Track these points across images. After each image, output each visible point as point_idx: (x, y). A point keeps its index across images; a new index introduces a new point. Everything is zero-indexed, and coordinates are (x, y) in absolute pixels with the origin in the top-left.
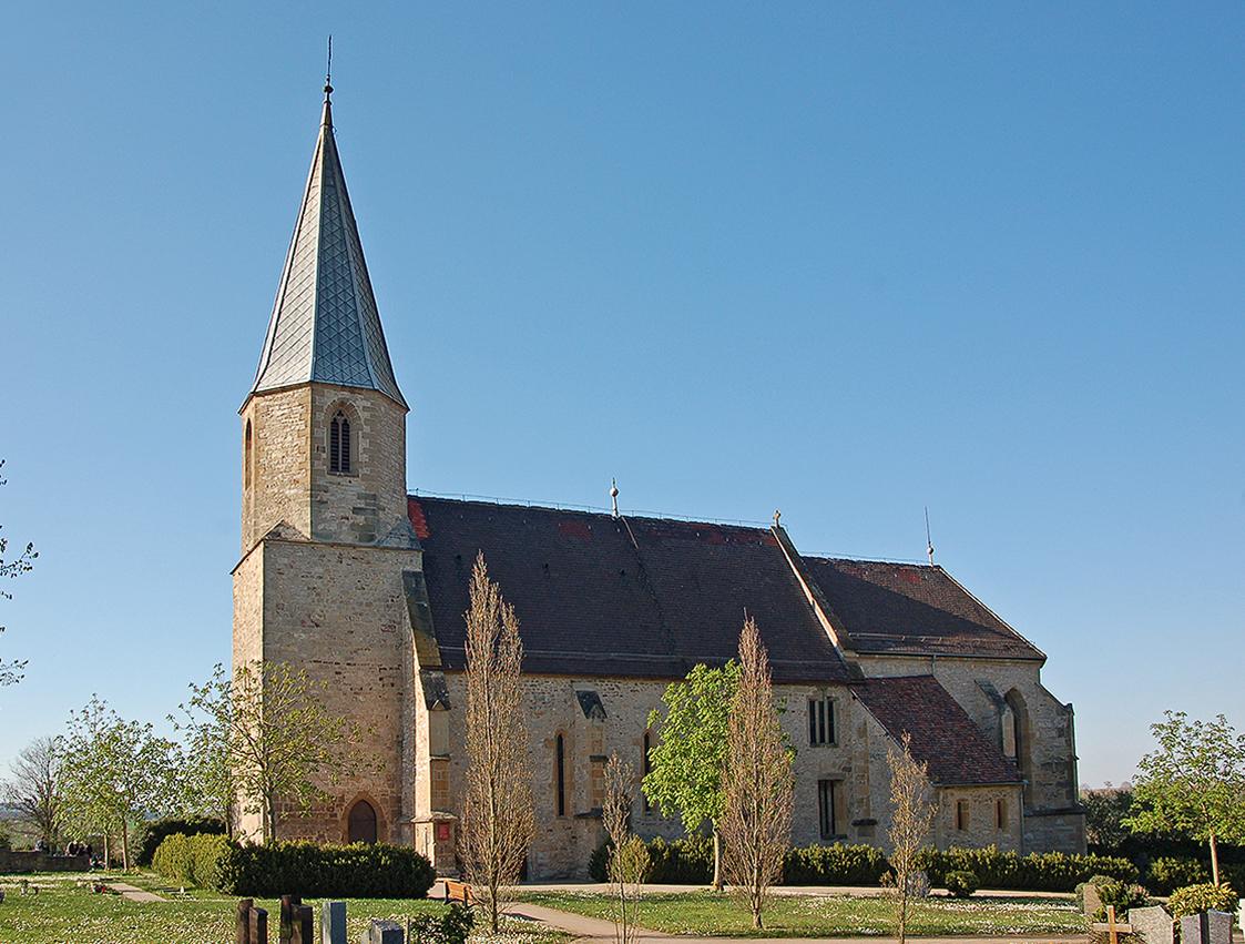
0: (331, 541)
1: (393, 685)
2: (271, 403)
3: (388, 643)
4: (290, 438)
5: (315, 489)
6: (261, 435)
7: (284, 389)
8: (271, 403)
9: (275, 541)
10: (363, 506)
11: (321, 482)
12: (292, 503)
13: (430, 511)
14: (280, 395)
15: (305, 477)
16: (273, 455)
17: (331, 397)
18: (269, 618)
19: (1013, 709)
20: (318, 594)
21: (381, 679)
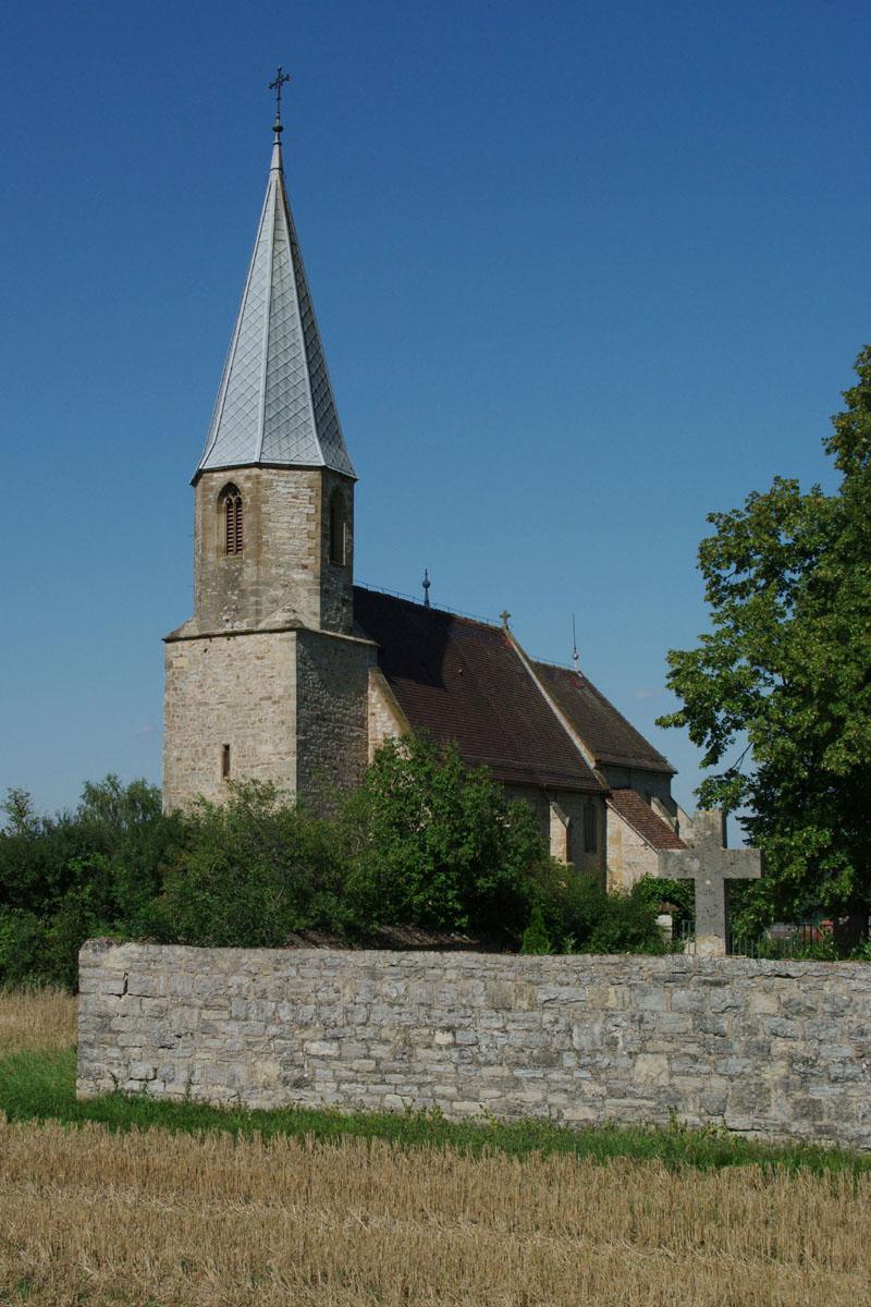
2: (276, 478)
14: (286, 472)
15: (314, 561)
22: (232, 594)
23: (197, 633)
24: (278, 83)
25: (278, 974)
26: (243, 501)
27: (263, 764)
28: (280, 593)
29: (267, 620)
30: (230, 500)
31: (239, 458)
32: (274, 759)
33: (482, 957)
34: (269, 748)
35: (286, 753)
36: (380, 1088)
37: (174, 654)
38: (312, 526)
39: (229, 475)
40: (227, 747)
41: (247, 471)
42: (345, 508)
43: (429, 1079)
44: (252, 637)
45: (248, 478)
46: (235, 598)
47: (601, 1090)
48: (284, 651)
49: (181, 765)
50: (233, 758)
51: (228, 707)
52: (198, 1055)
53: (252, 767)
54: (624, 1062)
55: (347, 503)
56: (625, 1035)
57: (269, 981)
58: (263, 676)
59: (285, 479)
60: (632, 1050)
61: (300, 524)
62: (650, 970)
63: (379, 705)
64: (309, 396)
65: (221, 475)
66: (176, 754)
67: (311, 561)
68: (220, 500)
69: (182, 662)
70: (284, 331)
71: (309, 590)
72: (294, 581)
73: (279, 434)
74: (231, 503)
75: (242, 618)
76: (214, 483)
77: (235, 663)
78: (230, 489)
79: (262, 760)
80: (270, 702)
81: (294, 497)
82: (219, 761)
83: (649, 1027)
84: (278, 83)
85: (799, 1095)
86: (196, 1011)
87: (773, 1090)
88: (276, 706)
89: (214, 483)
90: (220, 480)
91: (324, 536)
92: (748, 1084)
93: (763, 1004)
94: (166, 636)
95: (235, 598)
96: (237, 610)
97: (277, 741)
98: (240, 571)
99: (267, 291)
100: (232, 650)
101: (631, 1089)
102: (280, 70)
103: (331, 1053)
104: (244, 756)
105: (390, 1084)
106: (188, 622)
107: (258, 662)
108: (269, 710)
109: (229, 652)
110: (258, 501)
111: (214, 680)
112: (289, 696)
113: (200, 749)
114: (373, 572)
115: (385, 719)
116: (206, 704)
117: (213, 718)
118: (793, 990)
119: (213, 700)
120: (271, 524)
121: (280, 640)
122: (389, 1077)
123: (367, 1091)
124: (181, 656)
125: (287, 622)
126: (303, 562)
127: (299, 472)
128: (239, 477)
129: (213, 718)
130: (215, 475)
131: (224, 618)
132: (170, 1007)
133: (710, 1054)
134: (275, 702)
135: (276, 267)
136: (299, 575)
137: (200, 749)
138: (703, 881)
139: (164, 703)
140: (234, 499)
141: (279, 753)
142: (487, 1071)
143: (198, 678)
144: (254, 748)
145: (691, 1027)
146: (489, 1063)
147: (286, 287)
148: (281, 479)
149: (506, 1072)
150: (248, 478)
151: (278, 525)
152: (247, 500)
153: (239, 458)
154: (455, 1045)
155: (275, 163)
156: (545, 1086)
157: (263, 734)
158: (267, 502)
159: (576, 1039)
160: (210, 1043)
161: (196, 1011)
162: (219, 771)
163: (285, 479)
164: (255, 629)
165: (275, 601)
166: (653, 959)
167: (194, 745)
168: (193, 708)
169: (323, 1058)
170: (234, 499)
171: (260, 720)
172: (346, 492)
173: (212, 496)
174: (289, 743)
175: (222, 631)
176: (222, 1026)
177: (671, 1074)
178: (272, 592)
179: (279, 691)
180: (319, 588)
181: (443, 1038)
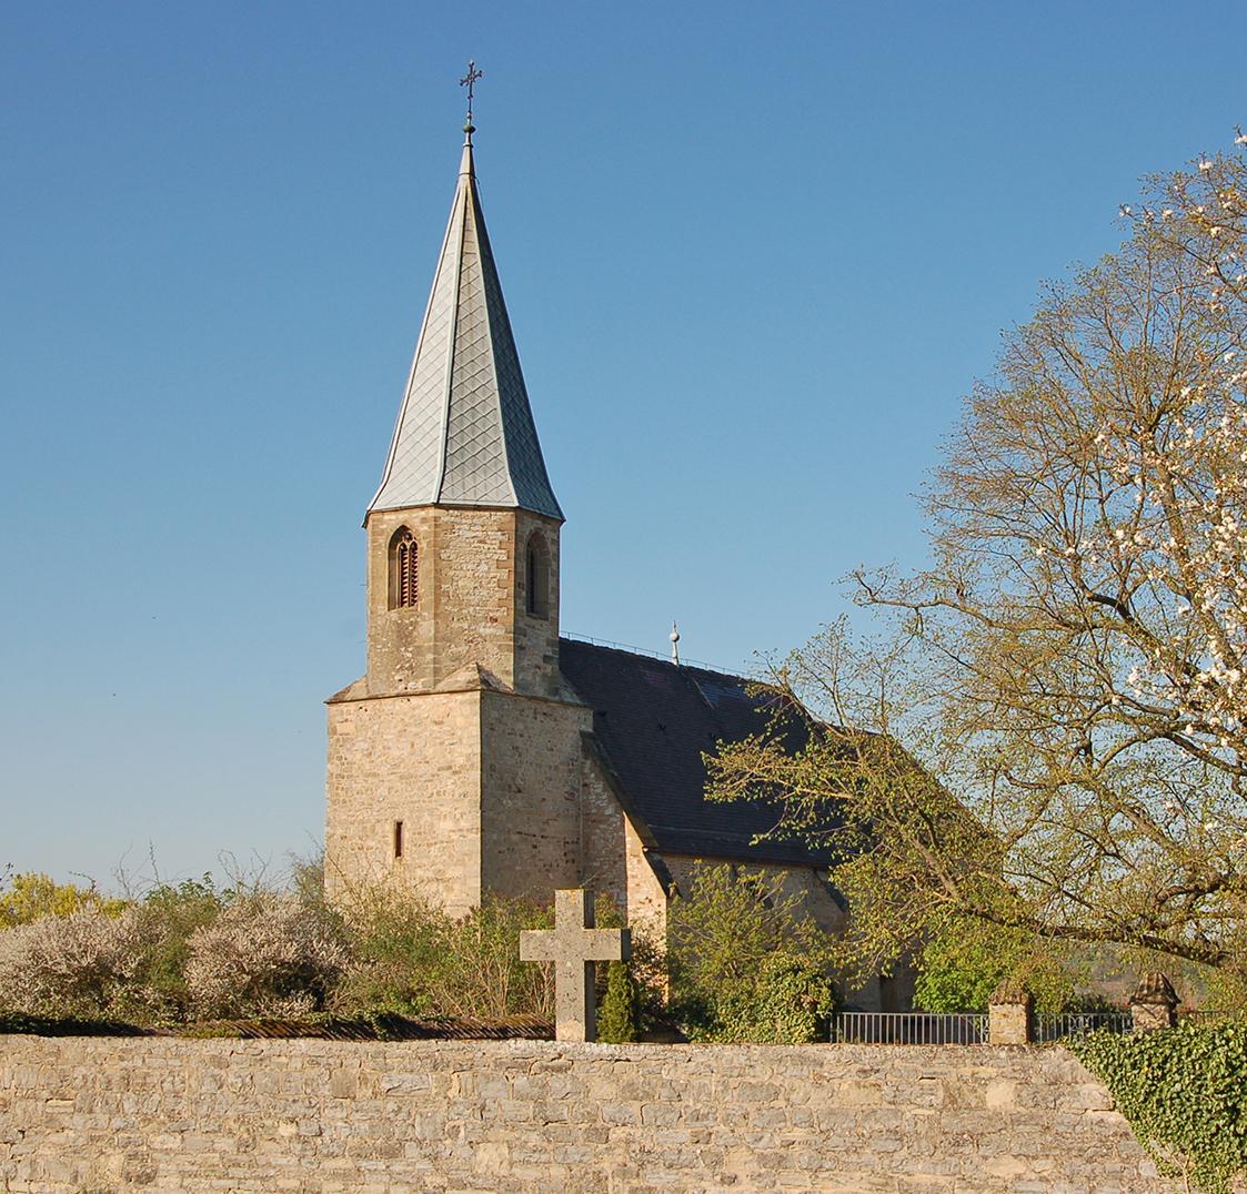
0: (528, 694)
1: (573, 861)
2: (458, 520)
3: (570, 812)
4: (484, 567)
5: (518, 632)
6: (443, 556)
7: (478, 508)
8: (458, 520)
9: (487, 688)
10: (550, 654)
11: (521, 625)
12: (488, 645)
13: (564, 642)
14: (470, 513)
15: (506, 615)
16: (461, 583)
17: (531, 525)
18: (484, 781)
19: (508, 694)
20: (520, 755)
21: (565, 854)
22: (406, 651)
23: (365, 696)
24: (471, 78)
25: (124, 1064)
26: (419, 546)
27: (442, 842)
28: (463, 649)
29: (447, 680)
30: (405, 546)
31: (412, 499)
32: (454, 837)
33: (328, 1043)
34: (447, 825)
35: (468, 830)
36: (224, 1183)
37: (339, 718)
38: (504, 574)
39: (402, 517)
40: (399, 824)
41: (423, 513)
42: (548, 553)
43: (272, 1172)
44: (429, 699)
45: (424, 520)
46: (410, 655)
47: (443, 1181)
48: (465, 715)
49: (346, 843)
50: (406, 835)
51: (401, 778)
52: (40, 1152)
53: (429, 845)
54: (467, 1152)
55: (552, 548)
56: (466, 1121)
57: (114, 1070)
58: (442, 743)
59: (469, 521)
60: (473, 1139)
61: (488, 572)
62: (492, 1056)
63: (593, 775)
64: (501, 428)
65: (393, 516)
66: (340, 832)
67: (500, 613)
68: (392, 546)
69: (349, 728)
70: (472, 355)
71: (500, 646)
72: (480, 636)
73: (463, 472)
74: (406, 550)
75: (417, 677)
76: (385, 526)
77: (408, 729)
78: (402, 531)
79: (440, 838)
80: (451, 771)
81: (480, 542)
82: (391, 838)
83: (491, 1115)
84: (471, 78)
85: (635, 1182)
86: (40, 1104)
87: (610, 1178)
88: (456, 777)
89: (385, 526)
90: (392, 522)
91: (517, 585)
92: (587, 1173)
93: (603, 1090)
94: (327, 699)
95: (410, 655)
96: (411, 667)
97: (458, 816)
98: (415, 624)
99: (452, 310)
100: (405, 714)
101: (471, 1179)
102: (471, 66)
103: (175, 1146)
104: (419, 833)
105: (232, 1178)
106: (356, 682)
107: (436, 728)
108: (449, 782)
109: (402, 716)
110: (438, 548)
111: (384, 747)
112: (472, 765)
113: (368, 825)
114: (581, 620)
115: (599, 791)
116: (375, 775)
117: (383, 791)
118: (630, 1074)
119: (384, 770)
120: (451, 573)
121: (461, 703)
122: (233, 1171)
123: (211, 1186)
124: (346, 720)
125: (469, 682)
126: (491, 615)
127: (487, 513)
128: (414, 520)
129: (383, 791)
130: (386, 517)
131: (397, 678)
132: (13, 1100)
133: (549, 1141)
134: (455, 773)
135: (463, 283)
136: (487, 630)
137: (368, 825)
138: (563, 964)
139: (327, 774)
140: (408, 545)
141: (460, 830)
142: (330, 1164)
143: (366, 746)
144: (432, 825)
145: (531, 1115)
146: (332, 1155)
147: (475, 306)
148: (464, 521)
149: (350, 1165)
150: (424, 520)
151: (461, 574)
152: (423, 545)
153: (412, 499)
154: (298, 1136)
155: (465, 167)
156: (386, 1178)
157: (442, 809)
158: (448, 547)
159: (418, 1129)
160: (55, 1138)
161: (40, 1104)
162: (391, 851)
163: (469, 521)
164: (432, 691)
165: (456, 658)
166: (495, 1044)
167: (362, 822)
168: (359, 780)
169: (167, 1152)
170: (408, 545)
171: (438, 793)
172: (549, 535)
173: (384, 541)
174: (473, 819)
175: (394, 693)
176: (66, 1120)
177: (511, 1164)
178: (454, 649)
179: (461, 761)
180: (512, 643)
181: (287, 1130)
